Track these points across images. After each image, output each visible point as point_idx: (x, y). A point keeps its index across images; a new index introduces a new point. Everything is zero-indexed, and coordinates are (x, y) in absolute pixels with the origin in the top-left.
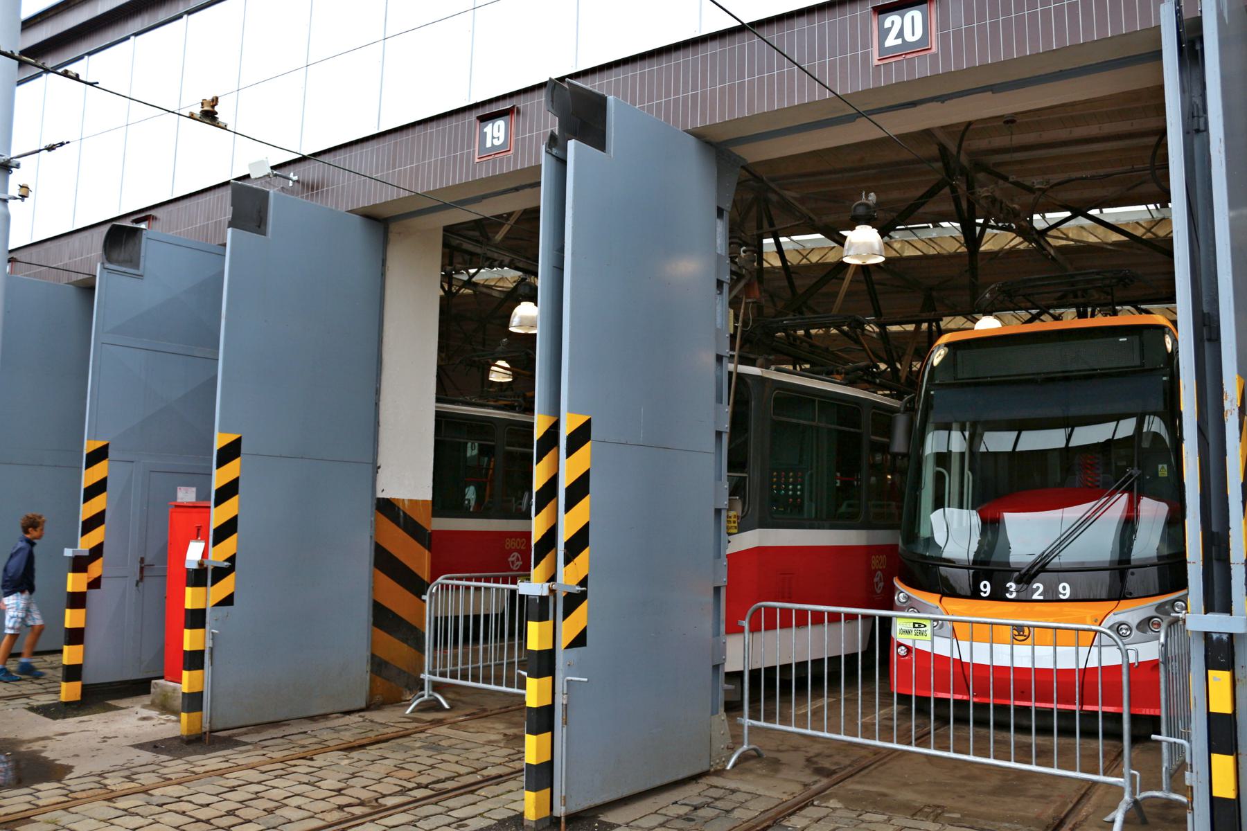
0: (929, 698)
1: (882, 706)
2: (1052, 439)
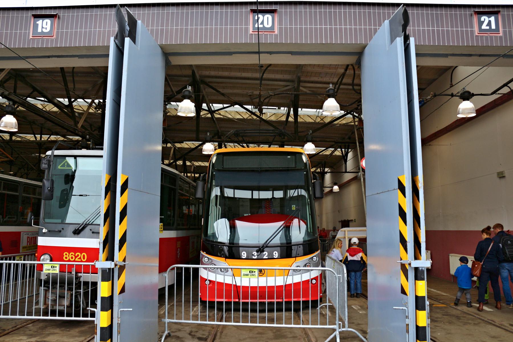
0: (231, 302)
1: (194, 306)
2: (246, 194)
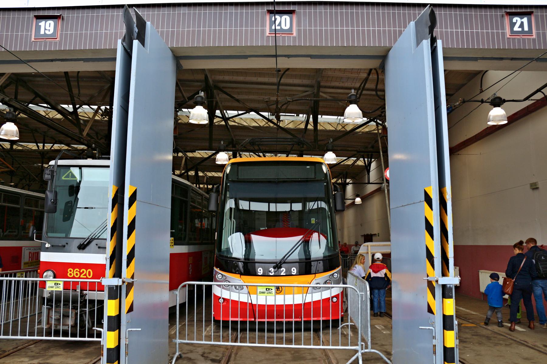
0: (247, 321)
1: (206, 326)
2: (262, 207)
